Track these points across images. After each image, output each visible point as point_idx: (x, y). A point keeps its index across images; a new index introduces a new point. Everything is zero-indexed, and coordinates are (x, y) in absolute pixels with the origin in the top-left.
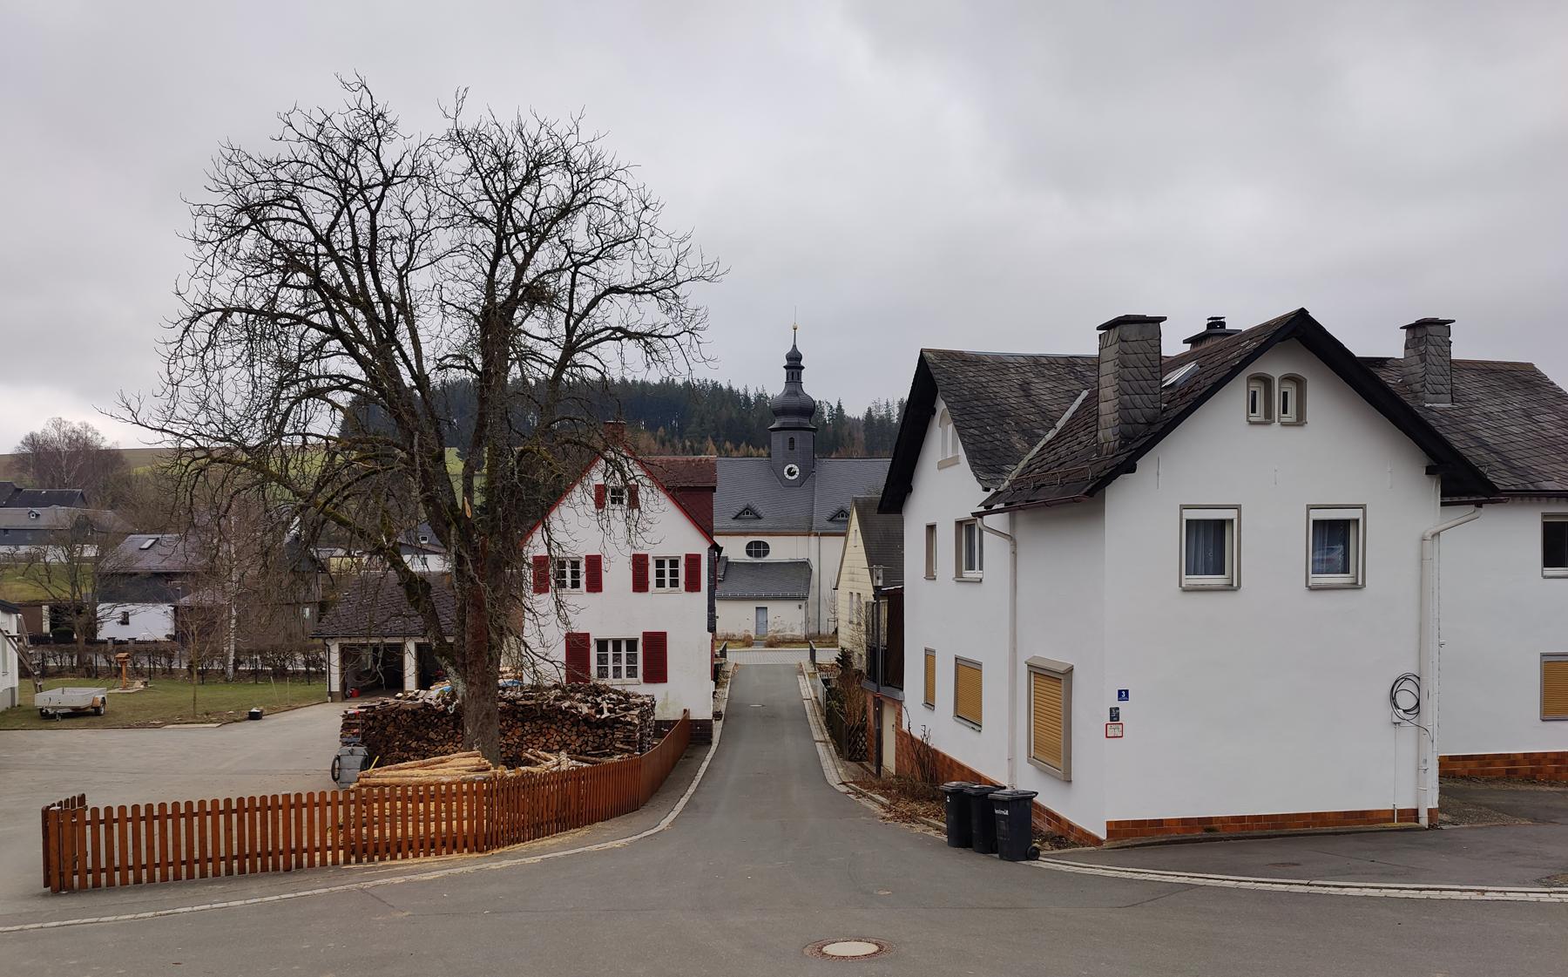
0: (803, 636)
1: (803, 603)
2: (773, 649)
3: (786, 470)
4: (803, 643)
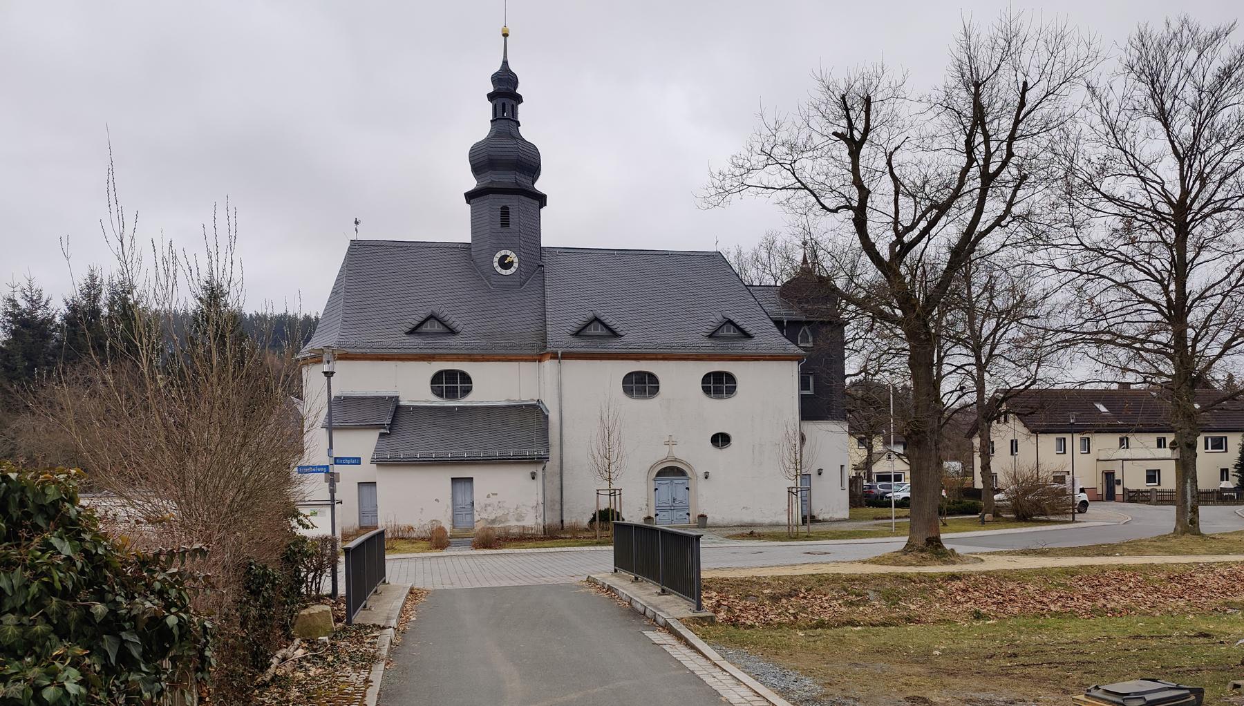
2: (494, 551)
3: (496, 260)
4: (540, 539)
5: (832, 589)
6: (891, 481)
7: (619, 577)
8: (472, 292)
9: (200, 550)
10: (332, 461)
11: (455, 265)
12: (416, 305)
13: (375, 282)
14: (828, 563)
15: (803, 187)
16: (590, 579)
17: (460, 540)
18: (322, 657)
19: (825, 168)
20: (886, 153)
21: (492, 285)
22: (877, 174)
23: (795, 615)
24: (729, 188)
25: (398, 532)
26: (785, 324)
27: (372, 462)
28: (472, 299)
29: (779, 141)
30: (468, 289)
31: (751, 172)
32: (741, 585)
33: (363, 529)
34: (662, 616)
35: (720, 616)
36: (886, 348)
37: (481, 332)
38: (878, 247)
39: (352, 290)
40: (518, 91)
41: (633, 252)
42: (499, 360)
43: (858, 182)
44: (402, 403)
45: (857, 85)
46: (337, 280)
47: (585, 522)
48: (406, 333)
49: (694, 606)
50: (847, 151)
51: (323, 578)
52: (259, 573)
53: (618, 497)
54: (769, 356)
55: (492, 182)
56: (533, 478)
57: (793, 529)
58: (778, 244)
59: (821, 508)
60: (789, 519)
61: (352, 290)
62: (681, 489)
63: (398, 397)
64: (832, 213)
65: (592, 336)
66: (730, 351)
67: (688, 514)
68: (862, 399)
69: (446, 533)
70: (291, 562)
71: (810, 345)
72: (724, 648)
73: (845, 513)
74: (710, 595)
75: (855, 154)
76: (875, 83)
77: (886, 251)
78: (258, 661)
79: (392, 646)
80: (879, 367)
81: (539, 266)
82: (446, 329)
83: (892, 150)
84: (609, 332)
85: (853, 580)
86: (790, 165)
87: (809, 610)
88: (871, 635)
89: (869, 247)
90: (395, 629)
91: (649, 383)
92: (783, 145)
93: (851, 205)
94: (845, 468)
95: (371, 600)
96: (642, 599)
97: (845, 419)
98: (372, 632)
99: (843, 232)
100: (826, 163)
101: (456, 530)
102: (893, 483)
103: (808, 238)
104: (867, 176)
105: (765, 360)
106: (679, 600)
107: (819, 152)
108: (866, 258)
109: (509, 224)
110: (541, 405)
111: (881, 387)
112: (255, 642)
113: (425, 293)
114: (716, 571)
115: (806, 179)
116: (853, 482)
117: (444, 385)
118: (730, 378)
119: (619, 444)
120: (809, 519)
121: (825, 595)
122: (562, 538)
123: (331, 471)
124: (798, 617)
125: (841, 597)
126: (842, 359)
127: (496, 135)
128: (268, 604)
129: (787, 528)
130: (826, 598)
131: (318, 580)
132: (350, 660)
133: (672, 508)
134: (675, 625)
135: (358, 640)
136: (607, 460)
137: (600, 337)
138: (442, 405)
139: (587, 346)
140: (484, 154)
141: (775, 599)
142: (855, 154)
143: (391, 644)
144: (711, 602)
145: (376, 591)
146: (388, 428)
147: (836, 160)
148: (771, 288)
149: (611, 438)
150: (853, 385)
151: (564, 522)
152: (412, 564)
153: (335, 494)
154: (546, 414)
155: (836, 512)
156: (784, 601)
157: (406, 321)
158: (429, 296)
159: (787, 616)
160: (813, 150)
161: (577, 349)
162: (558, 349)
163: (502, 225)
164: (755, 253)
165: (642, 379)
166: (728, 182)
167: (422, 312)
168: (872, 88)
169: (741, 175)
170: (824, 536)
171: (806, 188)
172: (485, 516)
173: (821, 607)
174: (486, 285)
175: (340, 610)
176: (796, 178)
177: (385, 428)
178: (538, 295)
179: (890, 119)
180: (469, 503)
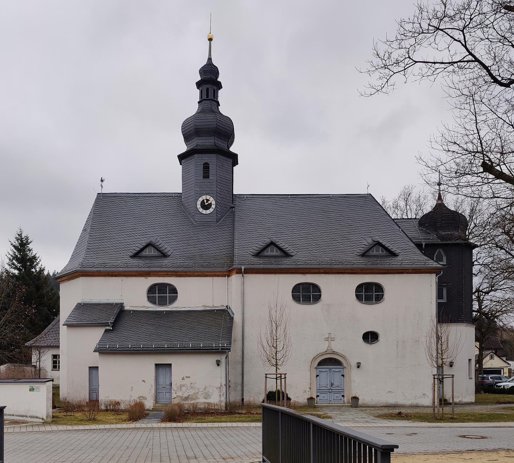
0: (223, 404)
1: (223, 358)
11: (170, 208)
12: (139, 237)
13: (112, 221)
26: (424, 246)
27: (95, 351)
28: (181, 232)
30: (178, 225)
37: (185, 255)
40: (218, 80)
41: (304, 196)
44: (127, 308)
48: (131, 257)
53: (283, 380)
55: (197, 145)
56: (218, 365)
62: (338, 376)
65: (269, 256)
66: (379, 266)
67: (343, 396)
73: (472, 398)
81: (231, 207)
82: (160, 253)
84: (282, 253)
101: (157, 405)
109: (209, 176)
110: (229, 310)
113: (147, 229)
122: (239, 413)
127: (201, 112)
133: (330, 391)
138: (155, 310)
139: (264, 264)
140: (192, 125)
146: (111, 325)
151: (245, 400)
155: (465, 397)
158: (149, 231)
162: (241, 266)
163: (204, 177)
172: (180, 394)
177: (109, 326)
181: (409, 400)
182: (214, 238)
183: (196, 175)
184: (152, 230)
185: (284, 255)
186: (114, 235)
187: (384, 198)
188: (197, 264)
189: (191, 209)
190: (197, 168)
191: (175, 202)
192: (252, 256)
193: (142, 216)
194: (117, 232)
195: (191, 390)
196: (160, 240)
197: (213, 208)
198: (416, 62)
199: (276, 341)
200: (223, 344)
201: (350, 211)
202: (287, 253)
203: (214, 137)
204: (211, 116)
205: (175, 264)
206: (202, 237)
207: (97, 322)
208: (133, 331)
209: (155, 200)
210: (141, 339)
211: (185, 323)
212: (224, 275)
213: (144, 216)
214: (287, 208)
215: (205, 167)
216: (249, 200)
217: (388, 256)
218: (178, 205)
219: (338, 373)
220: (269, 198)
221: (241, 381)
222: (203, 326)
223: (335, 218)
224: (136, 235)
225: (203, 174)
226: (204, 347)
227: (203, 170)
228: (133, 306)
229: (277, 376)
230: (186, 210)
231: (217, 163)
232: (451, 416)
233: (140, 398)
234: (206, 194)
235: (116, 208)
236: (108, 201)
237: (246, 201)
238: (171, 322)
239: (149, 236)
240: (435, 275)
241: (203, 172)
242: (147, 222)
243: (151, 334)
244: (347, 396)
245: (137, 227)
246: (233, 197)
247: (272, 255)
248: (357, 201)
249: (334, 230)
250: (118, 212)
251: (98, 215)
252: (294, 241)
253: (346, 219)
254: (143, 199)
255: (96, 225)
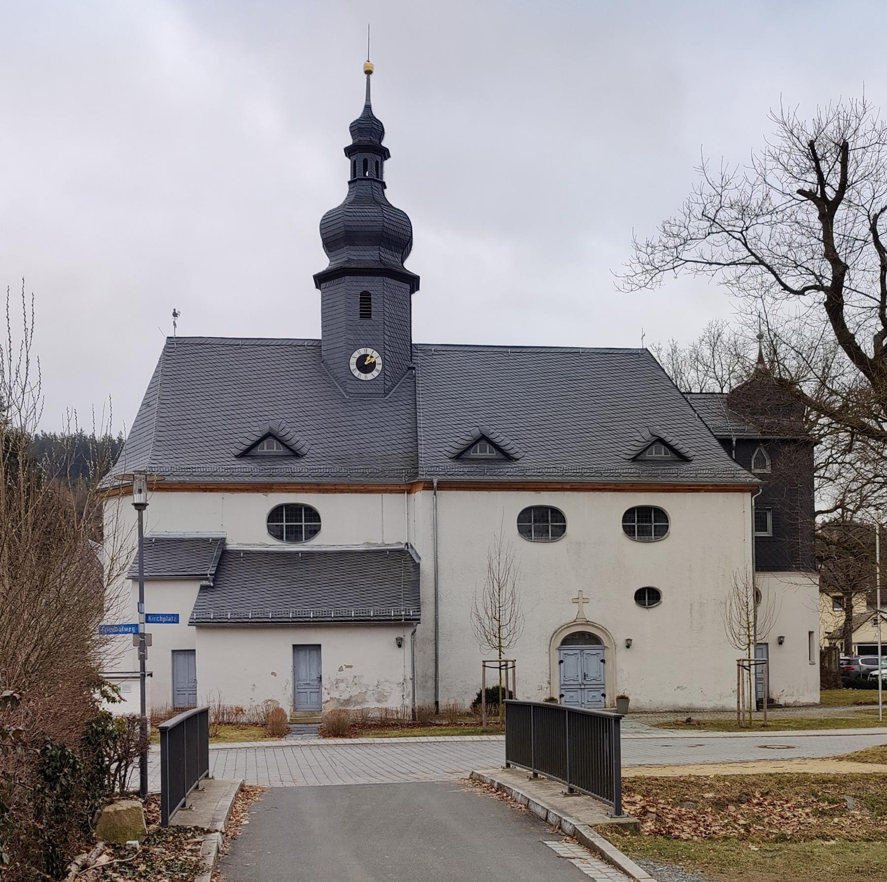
1: (407, 634)
2: (348, 741)
3: (353, 360)
4: (408, 725)
5: (797, 794)
6: (877, 654)
7: (513, 774)
8: (322, 403)
9: (11, 698)
10: (143, 619)
11: (301, 368)
12: (249, 420)
13: (198, 391)
14: (791, 760)
15: (757, 261)
16: (474, 776)
17: (303, 726)
18: (131, 865)
19: (787, 236)
20: (869, 216)
21: (348, 393)
22: (857, 243)
23: (746, 827)
24: (660, 264)
25: (223, 714)
26: (734, 443)
27: (191, 624)
28: (322, 412)
29: (726, 202)
30: (316, 399)
31: (689, 242)
32: (675, 787)
33: (177, 710)
34: (569, 825)
35: (646, 827)
36: (870, 476)
37: (332, 454)
38: (858, 340)
39: (168, 402)
42: (356, 491)
43: (831, 254)
45: (831, 127)
46: (149, 388)
47: (467, 703)
48: (236, 456)
49: (612, 809)
50: (817, 214)
51: (129, 769)
52: (56, 754)
53: (510, 671)
54: (712, 486)
55: (348, 261)
56: (400, 646)
57: (743, 715)
58: (725, 338)
59: (780, 690)
60: (739, 702)
61: (168, 402)
62: (594, 662)
63: (224, 539)
64: (797, 296)
65: (478, 459)
66: (660, 480)
67: (604, 695)
68: (838, 543)
69: (286, 716)
70: (93, 745)
71: (768, 470)
72: (652, 863)
73: (814, 695)
74: (633, 800)
75: (827, 218)
76: (853, 125)
77: (869, 344)
78: (53, 867)
79: (219, 855)
80: (861, 502)
81: (409, 368)
82: (287, 450)
83: (877, 212)
84: (500, 454)
85: (824, 782)
86: (741, 233)
87: (766, 820)
88: (849, 850)
89: (846, 340)
90: (223, 834)
91: (551, 522)
92: (731, 207)
93: (822, 285)
94: (815, 635)
95: (191, 797)
96: (543, 801)
97: (819, 571)
98: (193, 837)
99: (812, 320)
100: (789, 230)
102: (879, 657)
103: (764, 328)
104: (844, 246)
105: (706, 491)
106: (592, 803)
107: (780, 216)
108: (842, 355)
109: (370, 314)
110: (410, 550)
111: (866, 530)
112: (50, 841)
113: (261, 405)
114: (640, 768)
115: (762, 250)
116: (825, 655)
117: (284, 524)
118: (660, 515)
119: (513, 600)
120: (766, 703)
121: (787, 802)
122: (437, 725)
123: (141, 631)
124: (751, 829)
125: (808, 805)
126: (810, 490)
128: (66, 794)
129: (736, 714)
130: (789, 805)
131: (123, 773)
132: (167, 870)
133: (583, 687)
134: (588, 834)
135: (176, 846)
136: (496, 622)
137: (487, 460)
138: (282, 550)
141: (720, 805)
142: (827, 218)
143: (218, 852)
144: (633, 808)
145: (197, 787)
147: (802, 226)
148: (715, 396)
149: (503, 592)
150: (825, 525)
151: (439, 703)
152: (242, 755)
153: (146, 661)
154: (417, 562)
156: (732, 808)
157: (237, 440)
159: (736, 829)
160: (771, 213)
161: (458, 477)
163: (362, 316)
164: (695, 350)
165: (543, 516)
166: (658, 258)
167: (257, 429)
168: (851, 131)
169: (676, 247)
170: (786, 725)
171: (762, 262)
172: (336, 695)
173: (782, 817)
174: (340, 394)
175: (150, 811)
176: (749, 250)
177: (207, 579)
178: (408, 407)
179: (875, 171)
180: (315, 678)
181: (711, 701)
182: (382, 424)
183: (348, 313)
184: (271, 408)
185: (503, 457)
186: (203, 415)
187: (674, 342)
188: (354, 471)
189: (339, 370)
190: (349, 301)
191: (309, 355)
192: (450, 458)
193: (251, 381)
194: (208, 410)
195: (354, 688)
196: (287, 426)
197: (377, 370)
198: (687, 261)
199: (499, 610)
200: (407, 611)
201: (614, 379)
202: (508, 454)
203: (378, 247)
204: (373, 211)
205: (317, 471)
206: (359, 422)
207: (185, 573)
208: (249, 588)
209: (273, 351)
210: (267, 602)
211: (338, 574)
212: (402, 490)
213: (255, 380)
214: (507, 371)
215: (363, 298)
216: (440, 355)
217: (676, 461)
218: (314, 363)
219: (596, 656)
220: (475, 352)
221: (434, 673)
222: (369, 579)
223: (588, 391)
224: (243, 415)
225: (361, 311)
226: (376, 616)
227: (361, 304)
228: (242, 542)
229: (500, 664)
230: (331, 371)
231: (386, 293)
232: (762, 723)
233: (267, 702)
234: (366, 346)
235: (202, 366)
236: (187, 352)
237: (434, 357)
238: (313, 572)
239: (266, 418)
240: (750, 494)
241: (361, 308)
242: (260, 392)
243: (282, 594)
244: (609, 695)
245: (245, 402)
246: (411, 347)
247: (483, 457)
248: (624, 361)
249: (587, 414)
250: (207, 374)
251: (171, 377)
252: (519, 433)
253: (607, 393)
254: (252, 350)
255: (168, 398)
